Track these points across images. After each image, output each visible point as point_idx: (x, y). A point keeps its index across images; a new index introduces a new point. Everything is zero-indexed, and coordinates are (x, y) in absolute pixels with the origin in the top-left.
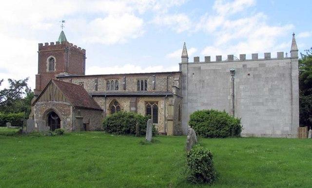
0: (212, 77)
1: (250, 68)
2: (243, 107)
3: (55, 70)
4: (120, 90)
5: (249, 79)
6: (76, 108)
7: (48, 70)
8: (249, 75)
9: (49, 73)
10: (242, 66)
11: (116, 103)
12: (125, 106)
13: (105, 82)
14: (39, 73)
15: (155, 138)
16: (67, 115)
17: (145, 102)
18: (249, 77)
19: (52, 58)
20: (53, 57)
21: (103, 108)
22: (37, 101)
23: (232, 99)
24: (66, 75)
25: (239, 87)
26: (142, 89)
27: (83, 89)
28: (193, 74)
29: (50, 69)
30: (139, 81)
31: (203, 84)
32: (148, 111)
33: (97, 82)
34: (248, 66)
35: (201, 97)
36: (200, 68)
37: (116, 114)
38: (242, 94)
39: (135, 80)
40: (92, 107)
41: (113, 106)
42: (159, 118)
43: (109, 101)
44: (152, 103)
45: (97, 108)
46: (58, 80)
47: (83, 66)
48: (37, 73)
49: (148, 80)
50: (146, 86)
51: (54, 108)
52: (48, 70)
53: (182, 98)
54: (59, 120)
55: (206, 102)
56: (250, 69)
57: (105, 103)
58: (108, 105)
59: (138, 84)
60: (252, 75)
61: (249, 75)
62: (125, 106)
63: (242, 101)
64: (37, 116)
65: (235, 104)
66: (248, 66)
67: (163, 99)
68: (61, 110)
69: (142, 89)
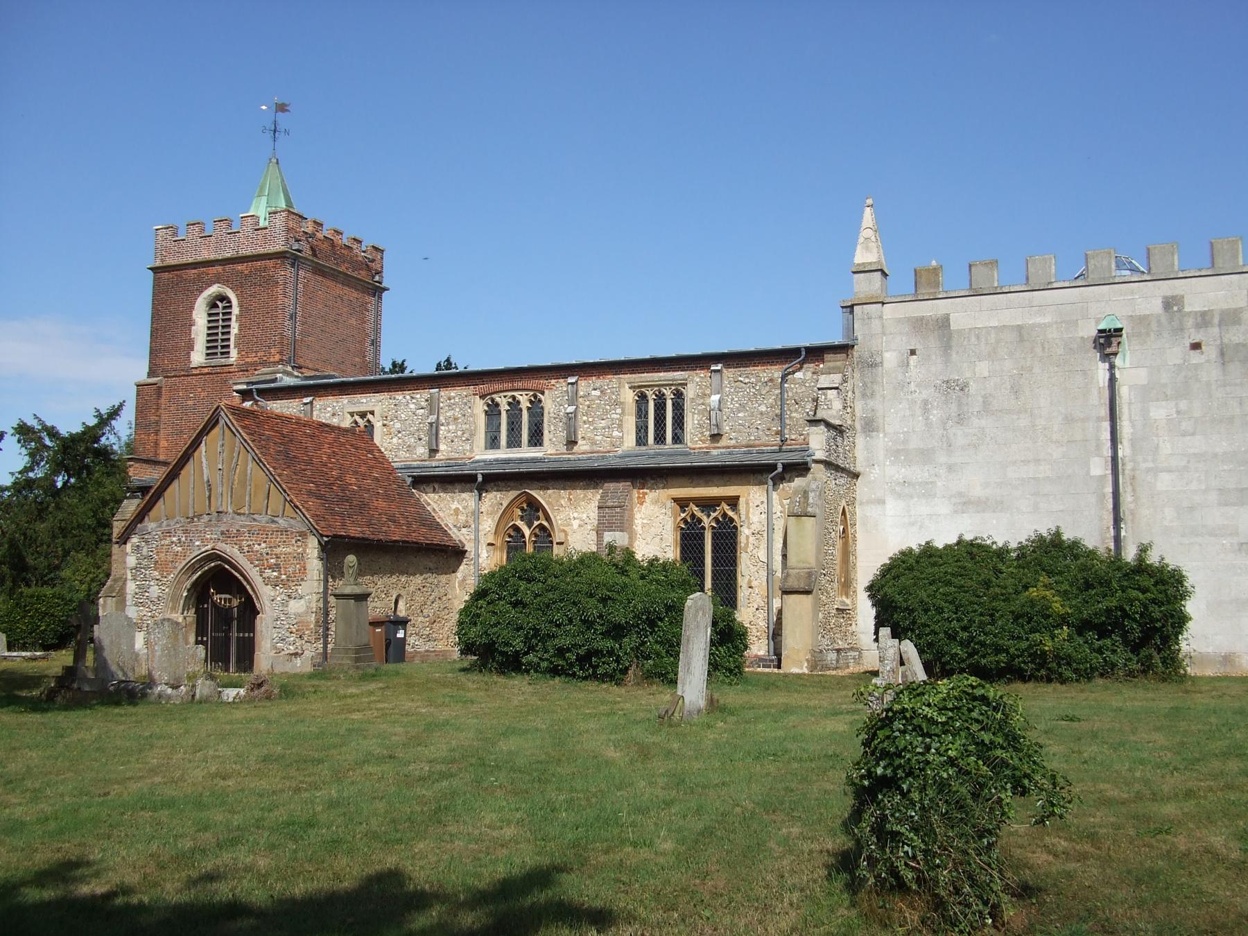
0: (1008, 364)
1: (1203, 314)
2: (1169, 512)
3: (234, 353)
4: (551, 450)
5: (1197, 367)
6: (333, 549)
7: (198, 357)
8: (1196, 346)
9: (200, 372)
10: (1156, 306)
11: (533, 508)
12: (576, 524)
13: (480, 406)
14: (151, 373)
15: (732, 696)
16: (288, 582)
17: (675, 500)
18: (1195, 357)
19: (223, 298)
20: (214, 289)
21: (461, 536)
22: (141, 516)
23: (1110, 478)
24: (288, 381)
25: (1145, 413)
26: (660, 438)
27: (372, 449)
28: (913, 352)
29: (211, 351)
30: (642, 398)
31: (960, 405)
32: (690, 539)
33: (433, 407)
34: (1193, 305)
35: (950, 468)
36: (943, 323)
37: (215, 362)
38: (1166, 448)
39: (624, 389)
40: (414, 537)
41: (517, 529)
42: (742, 582)
43: (496, 500)
44: (708, 504)
45: (421, 536)
46: (248, 404)
47: (369, 327)
48: (939, 544)
49: (690, 392)
50: (679, 422)
51: (230, 550)
52: (198, 357)
53: (856, 476)
54: (250, 610)
55: (977, 492)
56: (1204, 319)
57: (477, 514)
58: (488, 525)
59: (641, 413)
60: (1210, 351)
61: (1196, 346)
62: (576, 524)
63: (1164, 482)
64: (143, 589)
65: (1127, 498)
66: (1193, 305)
67: (761, 483)
68: (259, 561)
69: (660, 438)
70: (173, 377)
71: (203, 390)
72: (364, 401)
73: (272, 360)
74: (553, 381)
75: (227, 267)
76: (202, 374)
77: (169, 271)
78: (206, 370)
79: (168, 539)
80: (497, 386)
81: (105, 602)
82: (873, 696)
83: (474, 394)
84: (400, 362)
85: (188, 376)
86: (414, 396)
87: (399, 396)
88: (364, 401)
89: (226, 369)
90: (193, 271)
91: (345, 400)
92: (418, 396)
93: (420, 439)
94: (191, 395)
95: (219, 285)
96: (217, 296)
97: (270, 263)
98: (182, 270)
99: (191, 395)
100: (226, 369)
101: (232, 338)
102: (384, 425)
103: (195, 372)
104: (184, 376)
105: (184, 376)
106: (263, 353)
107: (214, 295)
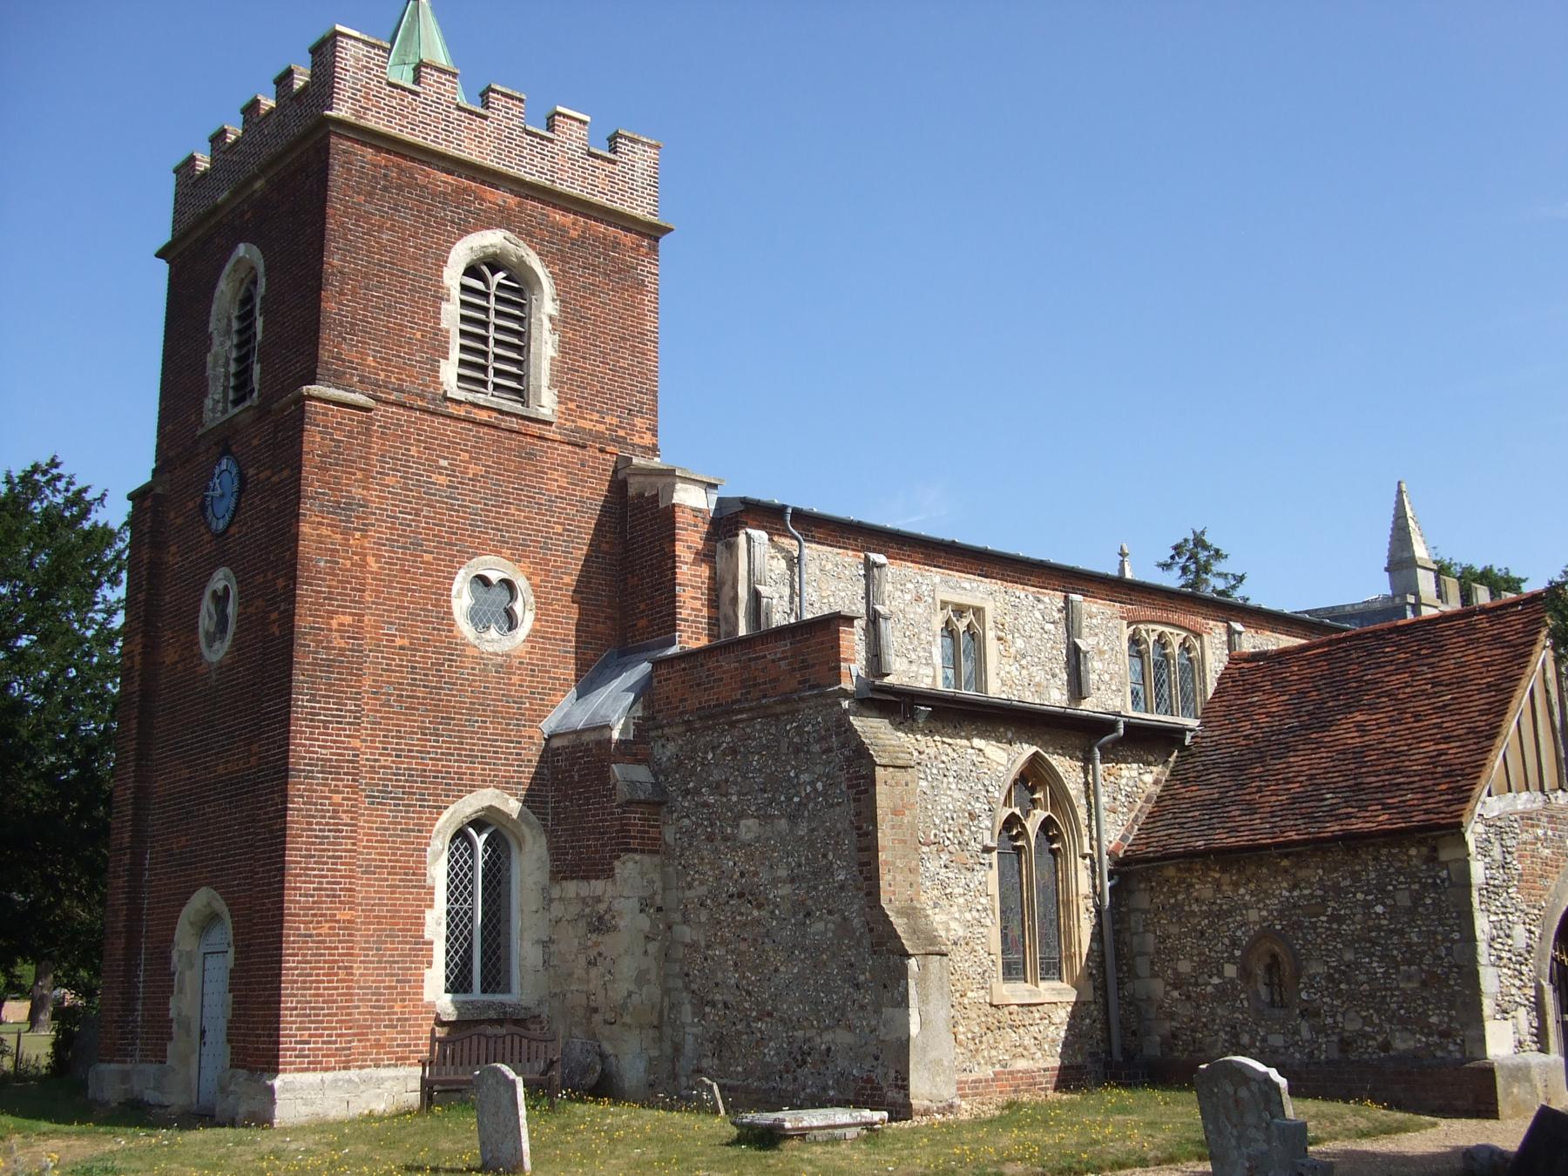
70: (393, 404)
71: (475, 459)
72: (967, 585)
73: (636, 440)
74: (1211, 623)
75: (530, 204)
76: (474, 422)
77: (378, 149)
78: (483, 416)
79: (1530, 830)
80: (1149, 613)
81: (923, 967)
82: (1119, 1139)
83: (1122, 618)
84: (58, 461)
85: (433, 413)
86: (1041, 597)
87: (1019, 591)
88: (967, 585)
89: (535, 429)
90: (444, 176)
91: (935, 576)
92: (1046, 599)
93: (1054, 676)
94: (443, 463)
95: (508, 234)
96: (486, 256)
97: (628, 239)
98: (413, 160)
99: (443, 463)
100: (535, 429)
101: (455, 354)
102: (1000, 639)
103: (453, 409)
104: (424, 410)
105: (424, 410)
106: (615, 421)
107: (491, 250)
